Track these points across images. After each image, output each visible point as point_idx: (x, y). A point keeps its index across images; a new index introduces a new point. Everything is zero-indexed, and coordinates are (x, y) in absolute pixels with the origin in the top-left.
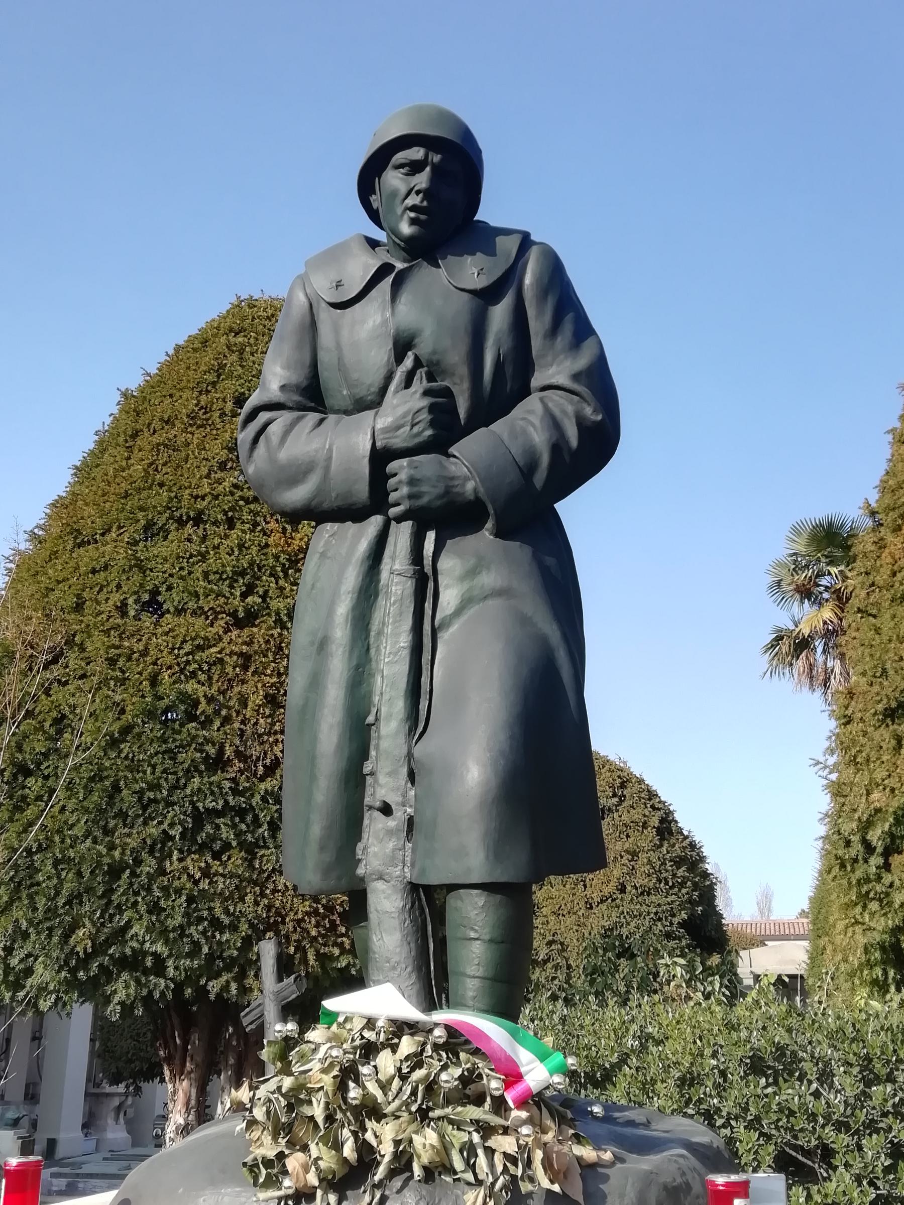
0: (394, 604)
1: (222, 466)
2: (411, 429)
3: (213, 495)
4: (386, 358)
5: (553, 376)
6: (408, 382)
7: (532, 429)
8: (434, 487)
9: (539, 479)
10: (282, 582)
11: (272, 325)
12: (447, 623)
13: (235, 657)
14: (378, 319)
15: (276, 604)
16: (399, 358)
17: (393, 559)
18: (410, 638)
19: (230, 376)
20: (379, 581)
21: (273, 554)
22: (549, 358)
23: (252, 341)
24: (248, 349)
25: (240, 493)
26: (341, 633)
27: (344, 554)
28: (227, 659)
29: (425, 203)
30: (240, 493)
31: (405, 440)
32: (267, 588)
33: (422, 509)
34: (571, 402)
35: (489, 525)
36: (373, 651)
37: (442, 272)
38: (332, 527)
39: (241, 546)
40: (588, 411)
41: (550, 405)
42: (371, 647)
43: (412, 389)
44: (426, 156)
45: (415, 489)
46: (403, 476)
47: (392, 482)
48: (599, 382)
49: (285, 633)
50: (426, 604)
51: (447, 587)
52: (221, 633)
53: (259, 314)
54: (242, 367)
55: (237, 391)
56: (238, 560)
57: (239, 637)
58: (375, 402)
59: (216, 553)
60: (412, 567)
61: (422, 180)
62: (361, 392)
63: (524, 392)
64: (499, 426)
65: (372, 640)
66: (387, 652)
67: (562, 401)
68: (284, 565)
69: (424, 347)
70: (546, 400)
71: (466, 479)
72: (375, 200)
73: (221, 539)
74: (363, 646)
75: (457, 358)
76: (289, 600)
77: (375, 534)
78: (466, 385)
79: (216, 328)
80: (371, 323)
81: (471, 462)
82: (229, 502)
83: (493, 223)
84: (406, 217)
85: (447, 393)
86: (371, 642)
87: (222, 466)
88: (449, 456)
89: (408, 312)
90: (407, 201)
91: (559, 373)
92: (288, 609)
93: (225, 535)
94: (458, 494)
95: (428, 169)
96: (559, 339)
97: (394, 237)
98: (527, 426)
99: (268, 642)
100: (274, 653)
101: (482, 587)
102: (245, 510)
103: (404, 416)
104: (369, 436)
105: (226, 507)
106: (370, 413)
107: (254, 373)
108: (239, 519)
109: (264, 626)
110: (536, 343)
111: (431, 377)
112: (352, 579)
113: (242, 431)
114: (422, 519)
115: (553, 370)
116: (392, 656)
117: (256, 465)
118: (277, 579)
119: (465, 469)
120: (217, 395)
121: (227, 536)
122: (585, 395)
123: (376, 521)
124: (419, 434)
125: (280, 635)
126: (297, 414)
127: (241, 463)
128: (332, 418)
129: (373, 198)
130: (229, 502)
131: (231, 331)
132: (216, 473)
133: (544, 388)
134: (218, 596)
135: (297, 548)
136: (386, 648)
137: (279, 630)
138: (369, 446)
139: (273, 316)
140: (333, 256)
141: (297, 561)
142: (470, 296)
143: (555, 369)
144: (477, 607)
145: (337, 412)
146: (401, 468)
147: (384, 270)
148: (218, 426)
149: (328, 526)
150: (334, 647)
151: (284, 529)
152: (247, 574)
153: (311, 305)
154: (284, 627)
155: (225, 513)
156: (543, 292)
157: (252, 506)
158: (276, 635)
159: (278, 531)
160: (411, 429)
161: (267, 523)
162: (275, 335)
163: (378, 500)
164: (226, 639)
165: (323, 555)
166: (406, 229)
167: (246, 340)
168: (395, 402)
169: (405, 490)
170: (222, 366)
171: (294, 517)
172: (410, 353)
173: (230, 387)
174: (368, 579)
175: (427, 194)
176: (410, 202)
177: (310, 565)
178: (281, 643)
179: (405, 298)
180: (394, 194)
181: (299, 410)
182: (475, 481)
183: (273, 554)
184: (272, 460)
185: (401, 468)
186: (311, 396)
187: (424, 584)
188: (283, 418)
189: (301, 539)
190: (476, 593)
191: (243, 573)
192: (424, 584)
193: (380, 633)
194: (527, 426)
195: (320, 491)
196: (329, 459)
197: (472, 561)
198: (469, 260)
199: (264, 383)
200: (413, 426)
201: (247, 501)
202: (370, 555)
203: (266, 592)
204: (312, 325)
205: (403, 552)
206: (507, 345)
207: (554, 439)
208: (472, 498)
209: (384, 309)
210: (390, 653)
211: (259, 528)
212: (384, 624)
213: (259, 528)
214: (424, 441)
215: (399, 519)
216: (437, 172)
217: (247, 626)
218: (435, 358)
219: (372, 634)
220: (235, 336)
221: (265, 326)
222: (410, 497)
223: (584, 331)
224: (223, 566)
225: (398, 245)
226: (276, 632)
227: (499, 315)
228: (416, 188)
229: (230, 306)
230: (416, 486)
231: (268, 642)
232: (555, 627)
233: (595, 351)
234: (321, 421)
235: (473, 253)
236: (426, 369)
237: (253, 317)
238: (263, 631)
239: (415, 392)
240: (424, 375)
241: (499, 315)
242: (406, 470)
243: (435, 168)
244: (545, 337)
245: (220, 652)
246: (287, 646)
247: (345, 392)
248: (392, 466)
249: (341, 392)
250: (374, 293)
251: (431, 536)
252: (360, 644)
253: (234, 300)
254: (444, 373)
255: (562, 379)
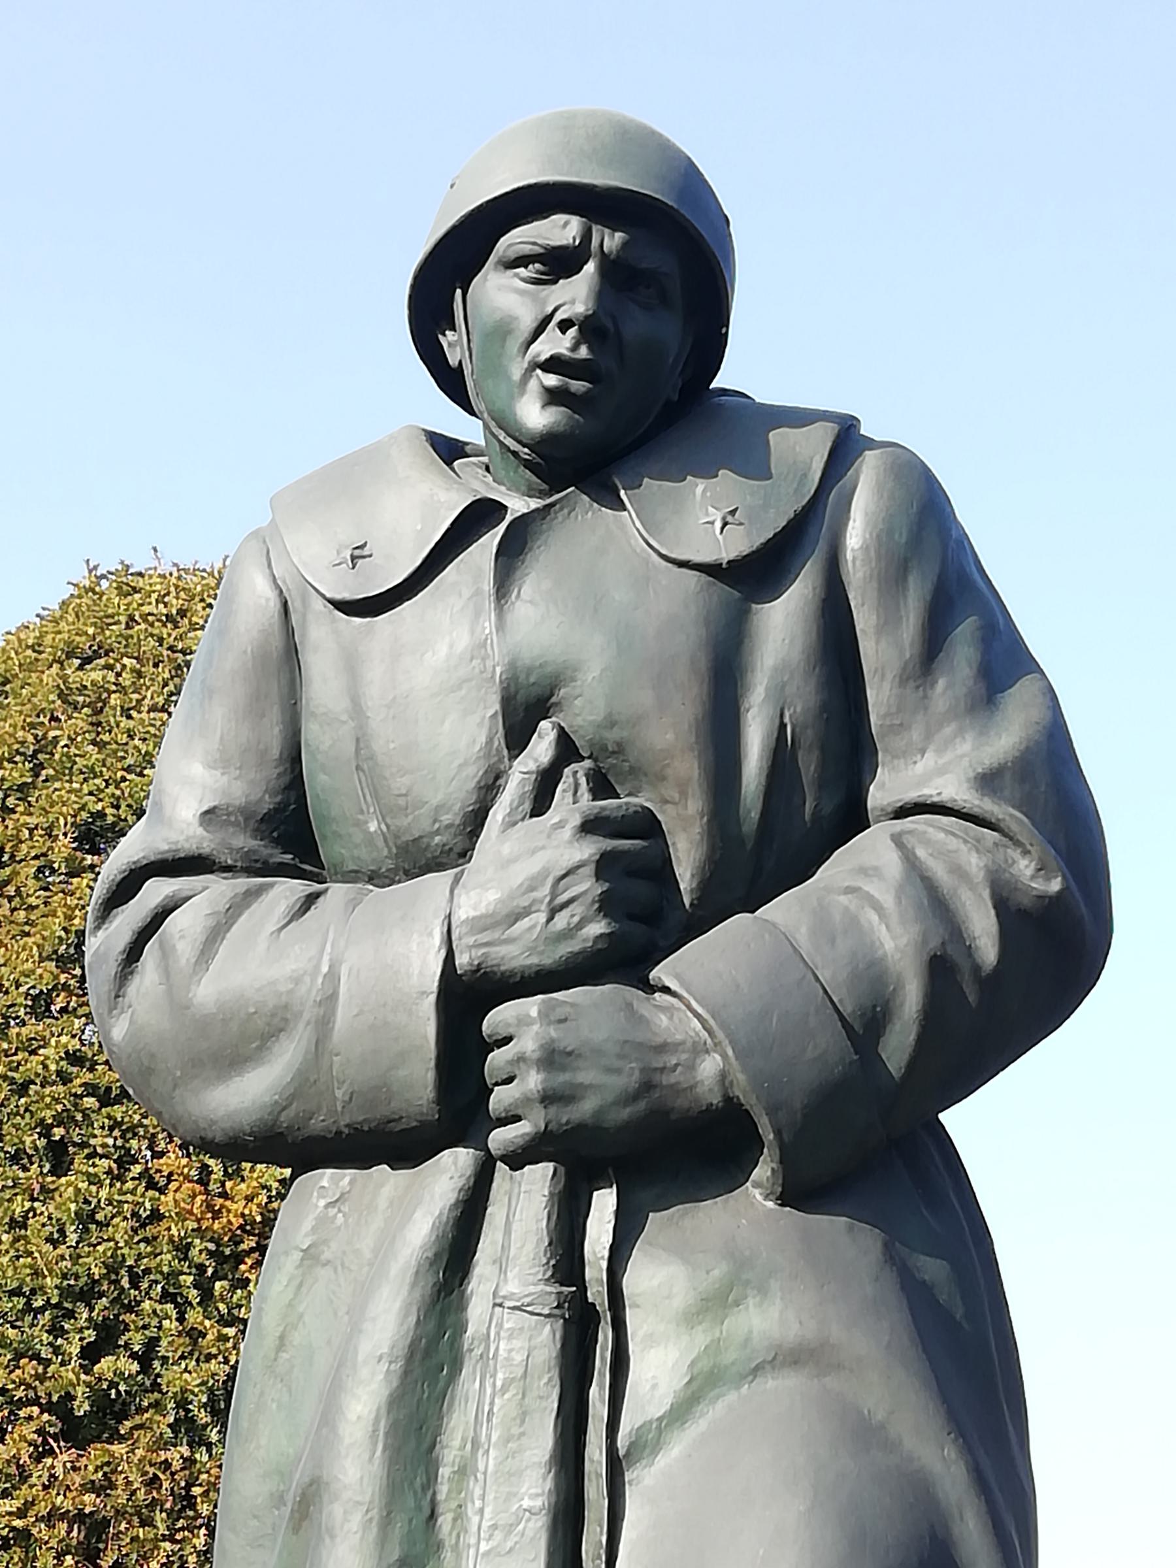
0: (504, 1389)
1: (40, 1005)
2: (550, 919)
3: (12, 1081)
4: (483, 739)
5: (925, 779)
6: (541, 800)
7: (874, 918)
8: (610, 1070)
9: (897, 1047)
10: (194, 1316)
11: (181, 638)
12: (650, 1441)
13: (63, 1527)
14: (463, 640)
15: (183, 1377)
16: (517, 737)
17: (501, 1264)
18: (549, 1484)
19: (66, 770)
20: (461, 1328)
21: (171, 1240)
22: (916, 735)
23: (127, 679)
24: (115, 699)
25: (88, 1077)
26: (356, 1470)
27: (368, 1254)
28: (40, 1531)
29: (583, 352)
30: (88, 1077)
31: (532, 950)
32: (152, 1332)
33: (579, 1130)
34: (978, 846)
35: (763, 1171)
36: (445, 1521)
37: (629, 519)
38: (335, 1181)
39: (87, 1219)
40: (1024, 867)
41: (921, 853)
42: (441, 1508)
43: (552, 816)
44: (587, 236)
45: (563, 1078)
46: (527, 1043)
47: (497, 1059)
48: (1052, 795)
49: (202, 1456)
50: (594, 1391)
51: (651, 1340)
52: (25, 1458)
53: (146, 609)
54: (100, 745)
55: (82, 808)
56: (76, 1258)
57: (75, 1469)
58: (454, 850)
59: (16, 1240)
60: (554, 1289)
61: (576, 294)
62: (417, 824)
63: (852, 819)
64: (782, 909)
65: (443, 1490)
66: (485, 1525)
67: (953, 843)
68: (201, 1268)
69: (582, 711)
70: (907, 839)
71: (699, 1050)
72: (453, 344)
73: (33, 1199)
74: (419, 1508)
75: (670, 736)
76: (213, 1365)
77: (452, 1197)
78: (695, 805)
79: (32, 647)
80: (443, 650)
81: (713, 1003)
82: (57, 1101)
83: (763, 394)
84: (533, 384)
85: (647, 826)
86: (441, 1497)
87: (40, 1005)
88: (650, 988)
89: (542, 621)
90: (535, 348)
91: (941, 771)
92: (211, 1391)
93: (44, 1189)
94: (675, 1089)
95: (590, 267)
96: (941, 684)
97: (502, 436)
98: (861, 908)
99: (153, 1483)
100: (169, 1513)
101: (747, 1340)
102: (100, 1120)
103: (532, 886)
104: (437, 938)
105: (48, 1114)
106: (438, 881)
107: (130, 761)
108: (83, 1145)
109: (145, 1438)
110: (879, 696)
111: (601, 786)
112: (387, 1318)
113: (98, 928)
114: (580, 1158)
115: (927, 762)
116: (498, 1535)
117: (133, 1019)
118: (182, 1309)
119: (696, 1023)
120: (32, 821)
121: (47, 1193)
122: (1014, 827)
123: (453, 1166)
124: (569, 933)
125: (189, 1462)
126: (244, 883)
127: (92, 998)
128: (337, 892)
129: (448, 339)
130: (57, 1101)
131: (70, 655)
132: (24, 1024)
133: (902, 812)
134: (18, 1356)
135: (237, 1222)
136: (481, 1511)
137: (185, 1450)
138: (436, 968)
139: (182, 613)
140: (346, 479)
141: (238, 1259)
142: (704, 578)
143: (930, 761)
144: (732, 1397)
145: (351, 877)
146: (520, 1022)
147: (477, 517)
148: (32, 901)
149: (326, 1177)
150: (337, 1510)
151: (205, 1169)
152: (101, 1295)
153: (285, 605)
154: (198, 1440)
155: (46, 1130)
156: (895, 569)
157: (118, 1111)
158: (176, 1465)
159: (187, 1178)
160: (550, 919)
161: (158, 1155)
162: (191, 678)
163: (460, 1105)
164: (39, 1475)
165: (310, 1256)
166: (535, 416)
167: (111, 677)
168: (506, 849)
169: (533, 1081)
170: (45, 746)
171: (238, 1149)
172: (544, 725)
173: (65, 800)
174: (431, 1325)
175: (589, 328)
176: (545, 348)
177: (274, 1287)
178: (189, 1486)
179: (532, 584)
180: (502, 330)
181: (251, 871)
182: (724, 1056)
183: (171, 1240)
184: (178, 1005)
185: (520, 1022)
186: (286, 836)
187: (587, 1334)
188: (209, 894)
189: (249, 1199)
190: (729, 1357)
191: (88, 1295)
192: (587, 1334)
193: (464, 1471)
194: (861, 908)
195: (304, 1083)
196: (330, 1000)
197: (719, 1271)
198: (699, 490)
199: (158, 805)
200: (553, 913)
201: (106, 1099)
202: (437, 1255)
203: (152, 1344)
204: (287, 656)
205: (530, 1247)
206: (802, 702)
207: (934, 943)
208: (716, 1099)
209: (477, 614)
210: (494, 1527)
211: (137, 1169)
212: (476, 1444)
213: (137, 1169)
214: (582, 952)
215: (518, 1159)
216: (614, 273)
217: (98, 1439)
218: (612, 736)
219: (444, 1472)
220: (81, 668)
221: (161, 641)
222: (548, 1098)
223: (1005, 661)
224: (37, 1273)
225: (515, 454)
226: (175, 1455)
227: (782, 624)
228: (559, 316)
229: (72, 590)
230: (563, 1068)
231: (153, 1483)
232: (951, 1452)
233: (1038, 713)
234: (311, 900)
235: (709, 473)
236: (588, 763)
237: (131, 618)
238: (140, 1452)
239: (560, 825)
240: (583, 781)
241: (782, 624)
242: (536, 1027)
243: (610, 268)
244: (903, 680)
245: (21, 1513)
246: (206, 1494)
247: (373, 827)
248: (498, 1018)
249: (361, 825)
250: (450, 573)
251: (604, 1203)
252: (411, 1503)
253: (82, 577)
254: (637, 774)
255: (952, 787)
